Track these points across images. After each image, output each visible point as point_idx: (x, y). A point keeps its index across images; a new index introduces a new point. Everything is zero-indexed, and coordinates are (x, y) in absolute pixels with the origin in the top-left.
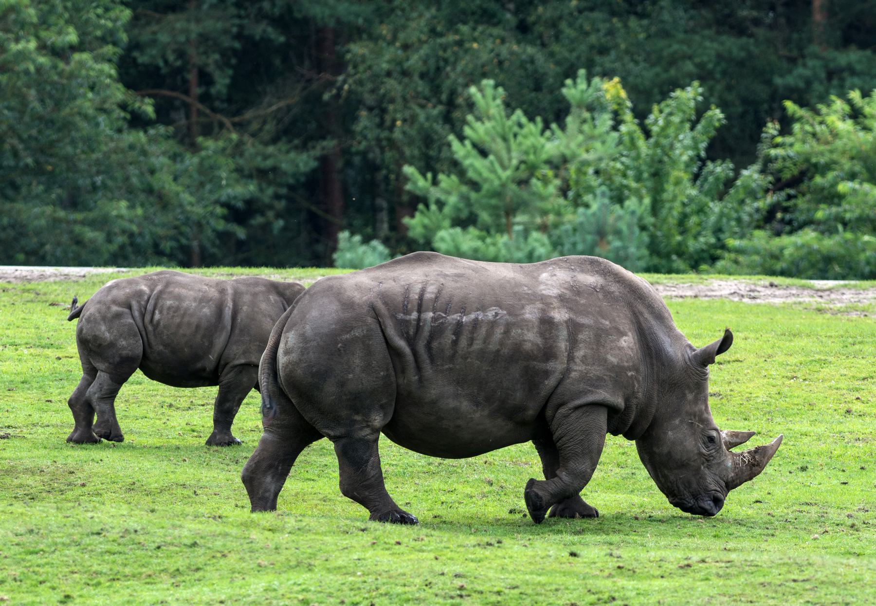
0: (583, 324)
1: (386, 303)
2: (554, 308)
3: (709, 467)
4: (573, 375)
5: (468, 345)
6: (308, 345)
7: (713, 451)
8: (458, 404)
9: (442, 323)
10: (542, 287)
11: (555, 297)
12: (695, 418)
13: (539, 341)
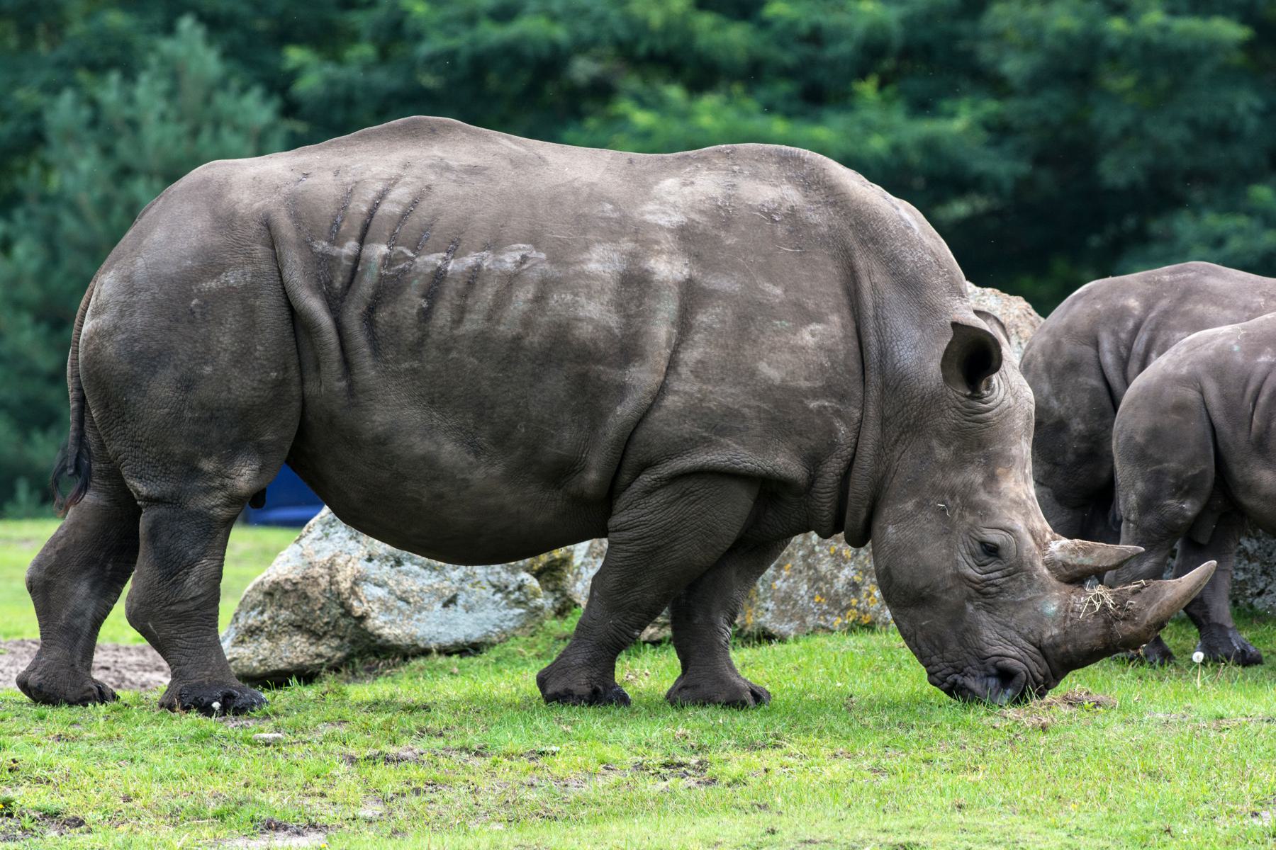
0: (715, 291)
1: (296, 217)
2: (660, 252)
3: (991, 608)
4: (671, 401)
5: (454, 321)
6: (135, 299)
7: (997, 574)
8: (433, 448)
9: (403, 271)
10: (650, 207)
11: (670, 231)
12: (952, 498)
13: (613, 321)
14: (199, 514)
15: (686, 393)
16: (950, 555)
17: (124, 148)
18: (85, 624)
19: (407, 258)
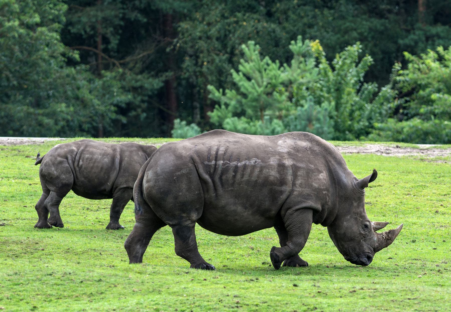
0: (300, 167)
1: (199, 156)
2: (285, 159)
3: (365, 241)
4: (295, 193)
5: (241, 178)
6: (159, 178)
7: (367, 232)
8: (236, 208)
9: (228, 166)
10: (279, 148)
11: (286, 153)
12: (358, 215)
13: (277, 175)
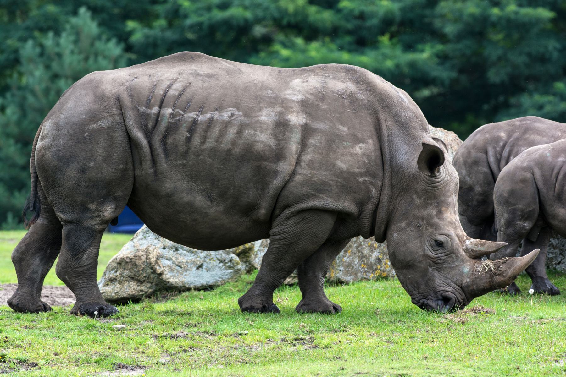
0: (317, 129)
1: (131, 96)
2: (293, 112)
3: (439, 270)
4: (298, 178)
5: (201, 143)
6: (60, 132)
7: (442, 255)
8: (192, 199)
9: (179, 120)
10: (288, 92)
11: (297, 102)
12: (422, 221)
13: (272, 142)
14: (88, 228)
15: (304, 174)
16: (422, 246)
17: (55, 66)
18: (38, 277)
19: (181, 115)
